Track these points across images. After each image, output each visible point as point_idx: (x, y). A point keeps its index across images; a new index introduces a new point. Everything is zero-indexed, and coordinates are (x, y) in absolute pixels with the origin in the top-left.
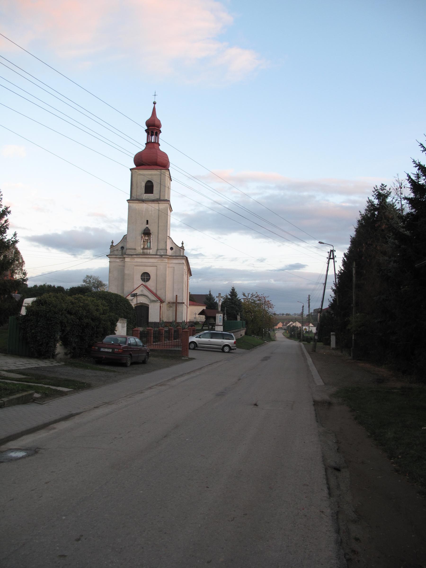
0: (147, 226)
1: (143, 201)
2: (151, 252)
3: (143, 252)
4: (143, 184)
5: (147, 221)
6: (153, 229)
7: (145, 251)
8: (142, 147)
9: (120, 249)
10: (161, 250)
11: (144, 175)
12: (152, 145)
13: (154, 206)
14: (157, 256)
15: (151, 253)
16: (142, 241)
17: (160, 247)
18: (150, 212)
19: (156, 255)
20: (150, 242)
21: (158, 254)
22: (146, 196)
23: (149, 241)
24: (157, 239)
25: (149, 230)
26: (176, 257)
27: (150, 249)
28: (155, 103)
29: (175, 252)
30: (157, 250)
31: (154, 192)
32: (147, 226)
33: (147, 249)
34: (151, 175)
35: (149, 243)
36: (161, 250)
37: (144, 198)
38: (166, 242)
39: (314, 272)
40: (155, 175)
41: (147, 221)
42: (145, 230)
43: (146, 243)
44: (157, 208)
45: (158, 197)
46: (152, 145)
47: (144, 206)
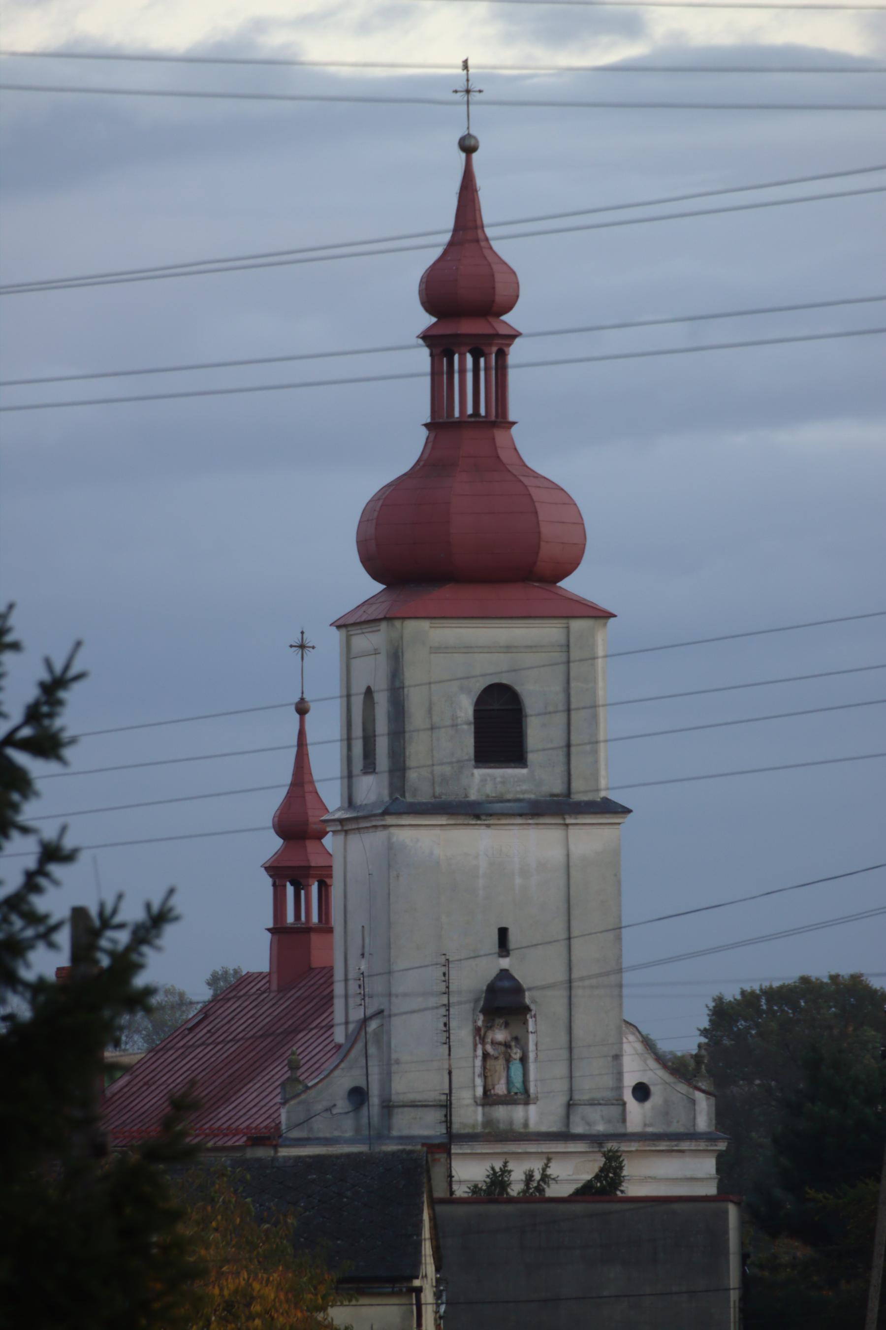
0: (505, 963)
1: (473, 812)
2: (537, 1116)
3: (488, 1122)
4: (466, 708)
5: (503, 933)
6: (534, 970)
7: (501, 1112)
8: (403, 446)
9: (342, 1105)
10: (592, 1103)
11: (468, 649)
12: (467, 436)
13: (533, 846)
14: (572, 1147)
15: (533, 1126)
16: (480, 1052)
17: (586, 1087)
18: (518, 881)
19: (565, 1136)
20: (524, 1060)
21: (578, 1128)
22: (484, 780)
23: (516, 1054)
24: (563, 1038)
25: (518, 990)
26: (672, 1145)
27: (525, 1097)
28: (468, 147)
29: (665, 1113)
30: (570, 1105)
31: (531, 757)
32: (505, 963)
33: (509, 1100)
34: (508, 649)
35: (516, 1070)
36: (592, 1103)
37: (473, 796)
38: (617, 1057)
39: (576, 593)
40: (532, 648)
41: (503, 933)
42: (492, 990)
43: (500, 1064)
44: (556, 854)
45: (558, 787)
46: (467, 436)
47: (476, 844)
